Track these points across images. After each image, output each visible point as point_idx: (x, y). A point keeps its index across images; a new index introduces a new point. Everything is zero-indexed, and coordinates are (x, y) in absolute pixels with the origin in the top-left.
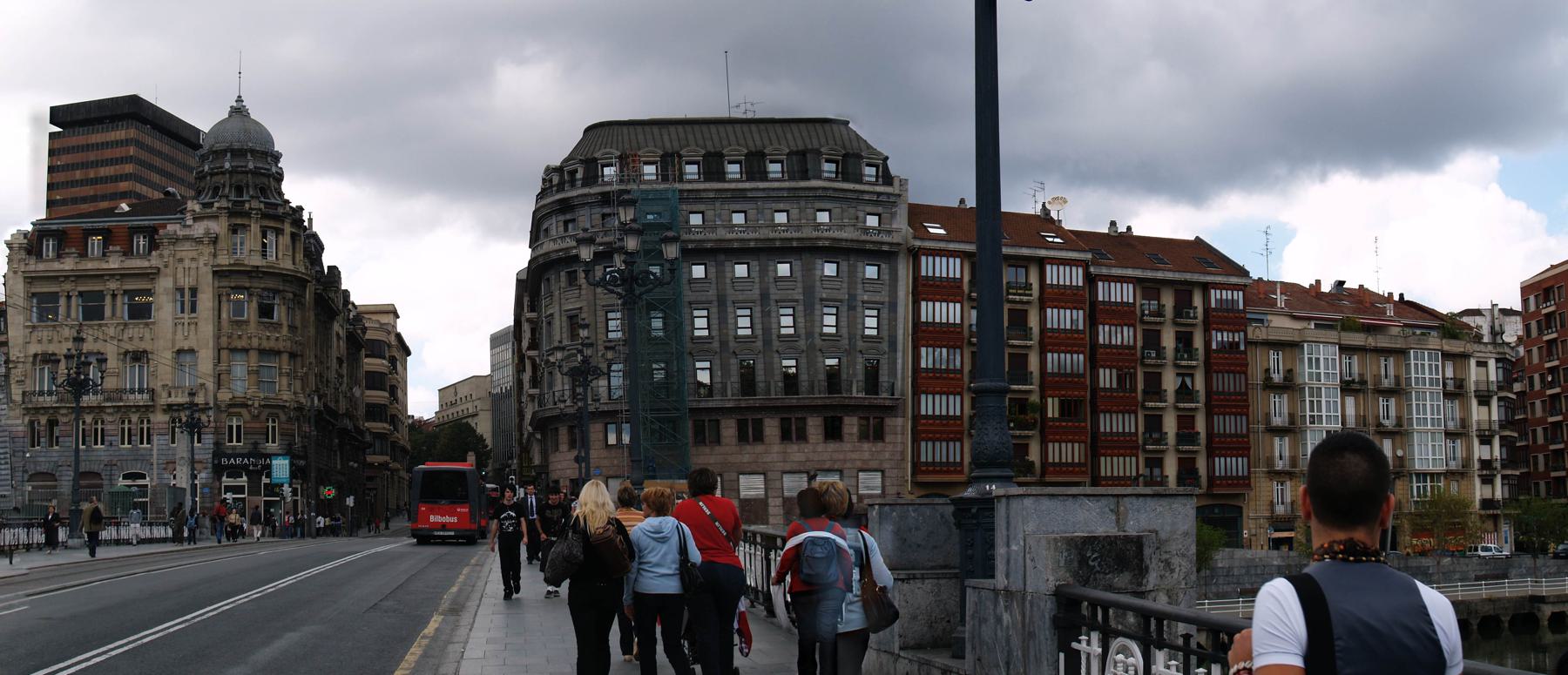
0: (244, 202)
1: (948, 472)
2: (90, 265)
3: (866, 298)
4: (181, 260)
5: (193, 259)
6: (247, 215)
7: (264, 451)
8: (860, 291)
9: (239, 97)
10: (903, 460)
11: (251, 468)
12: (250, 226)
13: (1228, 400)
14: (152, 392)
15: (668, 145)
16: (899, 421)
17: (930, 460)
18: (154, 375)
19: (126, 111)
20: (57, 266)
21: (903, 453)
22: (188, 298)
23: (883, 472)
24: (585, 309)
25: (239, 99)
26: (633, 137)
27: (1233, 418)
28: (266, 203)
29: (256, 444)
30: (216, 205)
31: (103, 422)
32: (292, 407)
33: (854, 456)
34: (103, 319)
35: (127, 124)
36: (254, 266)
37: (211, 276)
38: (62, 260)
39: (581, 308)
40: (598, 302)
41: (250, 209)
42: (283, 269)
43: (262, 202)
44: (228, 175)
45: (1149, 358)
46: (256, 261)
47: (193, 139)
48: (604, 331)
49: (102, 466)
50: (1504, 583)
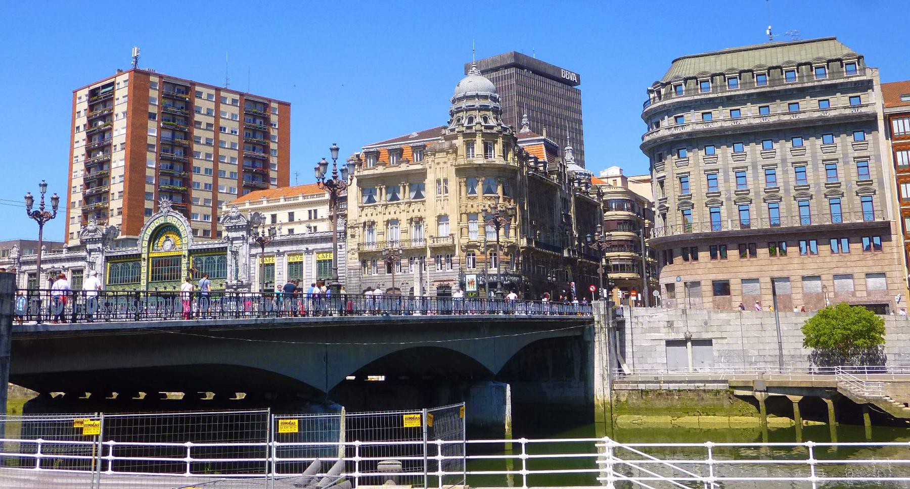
5: (445, 163)
30: (457, 130)
32: (506, 246)
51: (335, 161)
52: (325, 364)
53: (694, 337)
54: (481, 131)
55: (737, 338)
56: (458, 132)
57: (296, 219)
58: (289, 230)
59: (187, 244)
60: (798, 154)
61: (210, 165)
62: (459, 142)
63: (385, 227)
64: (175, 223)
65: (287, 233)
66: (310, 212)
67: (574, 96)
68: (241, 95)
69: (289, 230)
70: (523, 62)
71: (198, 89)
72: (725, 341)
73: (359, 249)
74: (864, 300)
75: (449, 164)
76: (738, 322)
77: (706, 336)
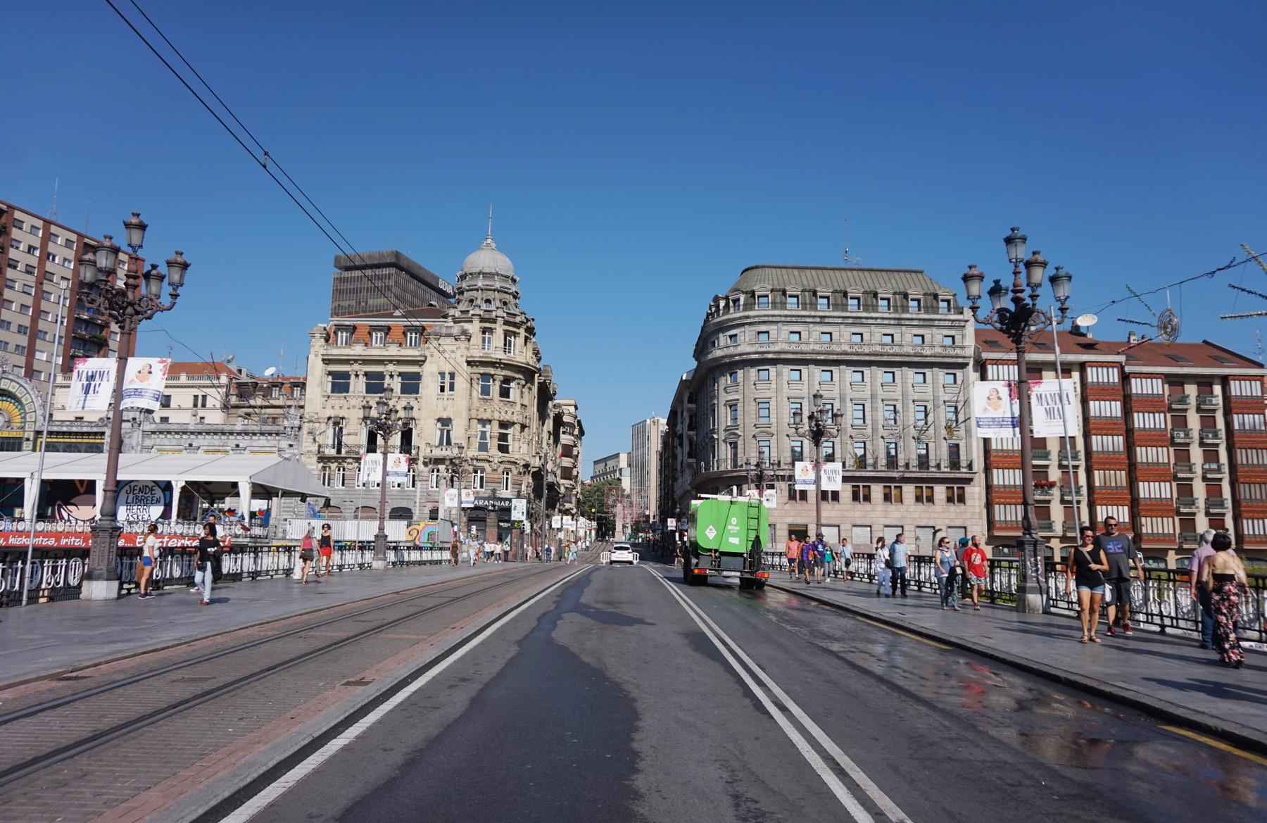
0: (491, 311)
2: (373, 352)
5: (453, 351)
6: (494, 321)
13: (1252, 472)
15: (805, 283)
17: (1003, 519)
22: (447, 384)
26: (780, 277)
27: (1257, 486)
28: (508, 313)
29: (494, 491)
30: (471, 312)
31: (344, 470)
33: (946, 515)
34: (348, 392)
38: (353, 348)
41: (497, 317)
45: (1179, 438)
46: (500, 355)
56: (473, 315)
57: (173, 404)
59: (35, 422)
61: (26, 322)
62: (474, 328)
64: (14, 391)
66: (196, 397)
68: (79, 235)
70: (403, 263)
71: (18, 215)
73: (319, 452)
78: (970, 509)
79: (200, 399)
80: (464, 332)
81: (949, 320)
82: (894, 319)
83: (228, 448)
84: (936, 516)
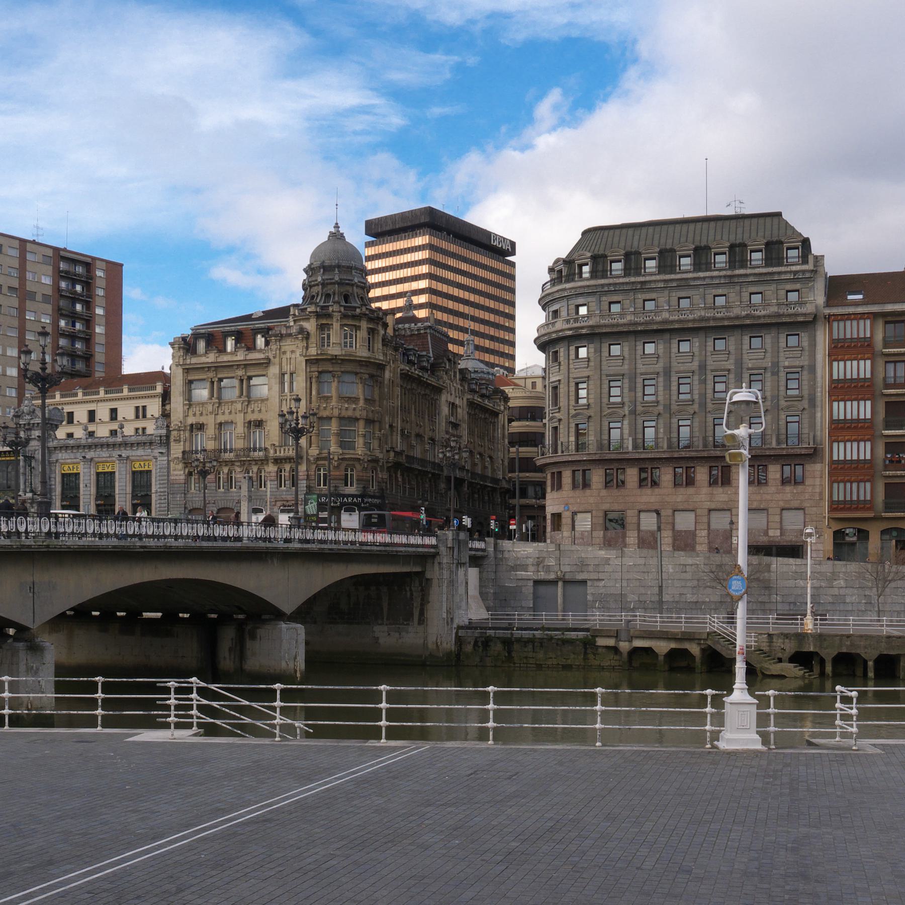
0: (328, 306)
1: (857, 509)
3: (787, 364)
4: (284, 353)
7: (342, 492)
8: (781, 359)
9: (337, 224)
10: (821, 499)
11: (363, 505)
12: (332, 325)
14: (266, 449)
16: (818, 467)
18: (267, 436)
19: (422, 221)
20: (203, 359)
21: (821, 494)
23: (658, 513)
24: (562, 382)
25: (337, 226)
30: (309, 310)
32: (366, 460)
35: (424, 231)
36: (332, 355)
37: (304, 363)
39: (559, 381)
40: (571, 375)
41: (333, 311)
42: (361, 357)
43: (342, 306)
44: (320, 286)
47: (485, 241)
48: (607, 396)
49: (234, 504)
50: (514, 615)
51: (43, 349)
52: (31, 595)
53: (567, 577)
54: (340, 312)
55: (616, 580)
58: (111, 431)
60: (718, 359)
63: (246, 430)
65: (107, 434)
66: (137, 408)
67: (507, 269)
69: (111, 431)
72: (602, 584)
74: (777, 540)
75: (298, 353)
76: (618, 562)
77: (580, 577)
78: (810, 489)
79: (141, 409)
80: (302, 330)
81: (791, 272)
82: (725, 276)
83: (114, 459)
84: (768, 497)
